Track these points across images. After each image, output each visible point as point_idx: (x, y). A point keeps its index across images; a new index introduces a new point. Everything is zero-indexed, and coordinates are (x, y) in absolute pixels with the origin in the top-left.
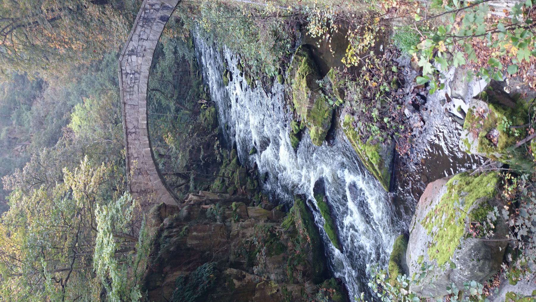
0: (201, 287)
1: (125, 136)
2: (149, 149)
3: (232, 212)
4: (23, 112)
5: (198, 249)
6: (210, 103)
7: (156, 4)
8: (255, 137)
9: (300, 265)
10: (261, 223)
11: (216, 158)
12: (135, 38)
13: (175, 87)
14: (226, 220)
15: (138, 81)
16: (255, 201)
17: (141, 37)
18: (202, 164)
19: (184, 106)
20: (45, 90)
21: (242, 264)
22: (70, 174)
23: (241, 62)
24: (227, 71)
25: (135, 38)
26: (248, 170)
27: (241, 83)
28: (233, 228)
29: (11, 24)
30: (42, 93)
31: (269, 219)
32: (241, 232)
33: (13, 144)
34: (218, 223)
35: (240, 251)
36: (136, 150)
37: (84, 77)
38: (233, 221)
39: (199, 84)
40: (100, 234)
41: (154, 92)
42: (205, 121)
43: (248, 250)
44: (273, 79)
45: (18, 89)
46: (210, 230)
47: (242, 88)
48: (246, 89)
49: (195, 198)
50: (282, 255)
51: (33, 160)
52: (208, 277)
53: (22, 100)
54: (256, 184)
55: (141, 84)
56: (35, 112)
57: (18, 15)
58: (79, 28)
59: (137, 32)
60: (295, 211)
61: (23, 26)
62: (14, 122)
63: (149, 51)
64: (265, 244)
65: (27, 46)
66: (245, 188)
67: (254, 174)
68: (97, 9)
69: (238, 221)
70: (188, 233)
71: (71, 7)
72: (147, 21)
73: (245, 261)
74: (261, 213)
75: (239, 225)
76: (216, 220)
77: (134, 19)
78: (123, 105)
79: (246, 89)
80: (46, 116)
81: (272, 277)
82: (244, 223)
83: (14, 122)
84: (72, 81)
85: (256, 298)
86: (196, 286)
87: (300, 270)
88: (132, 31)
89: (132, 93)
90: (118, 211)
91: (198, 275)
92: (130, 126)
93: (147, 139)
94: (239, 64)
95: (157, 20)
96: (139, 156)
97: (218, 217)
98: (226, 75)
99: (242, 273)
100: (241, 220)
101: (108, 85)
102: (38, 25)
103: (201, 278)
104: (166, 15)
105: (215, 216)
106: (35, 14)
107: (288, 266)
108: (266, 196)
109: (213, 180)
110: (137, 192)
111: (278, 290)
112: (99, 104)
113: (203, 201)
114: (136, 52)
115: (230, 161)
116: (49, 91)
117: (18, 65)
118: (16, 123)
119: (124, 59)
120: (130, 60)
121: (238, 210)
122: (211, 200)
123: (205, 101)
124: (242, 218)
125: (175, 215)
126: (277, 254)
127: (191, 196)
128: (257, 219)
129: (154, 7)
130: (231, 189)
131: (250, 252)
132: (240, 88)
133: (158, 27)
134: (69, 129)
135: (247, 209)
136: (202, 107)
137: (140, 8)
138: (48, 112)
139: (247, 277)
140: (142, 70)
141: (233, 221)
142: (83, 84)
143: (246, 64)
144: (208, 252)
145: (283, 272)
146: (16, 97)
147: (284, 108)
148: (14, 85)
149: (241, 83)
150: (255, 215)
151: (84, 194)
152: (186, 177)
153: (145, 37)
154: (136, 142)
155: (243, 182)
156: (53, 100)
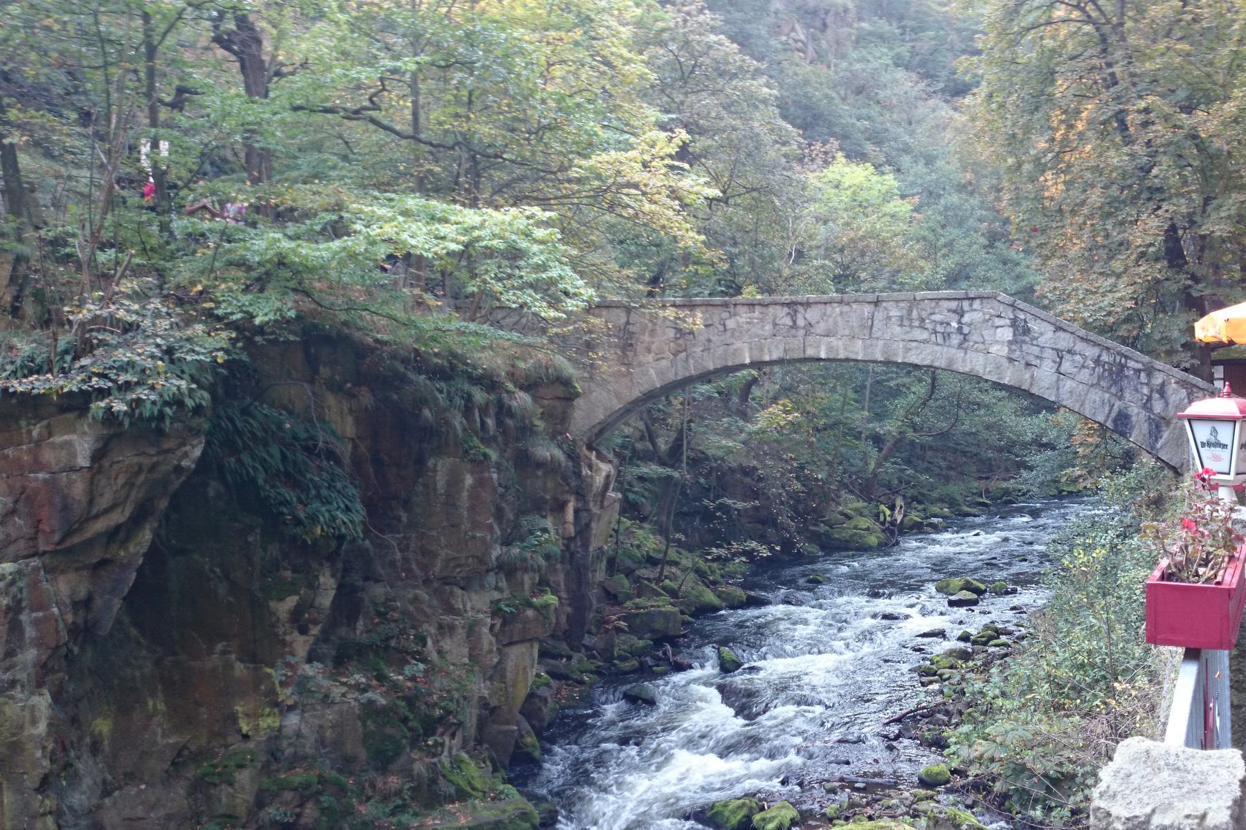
0: (290, 494)
1: (787, 298)
2: (747, 361)
3: (527, 593)
4: (891, 49)
5: (420, 488)
6: (892, 533)
7: (1167, 404)
8: (773, 668)
9: (317, 814)
10: (480, 688)
11: (718, 546)
12: (1064, 341)
13: (944, 435)
14: (502, 576)
15: (940, 340)
16: (574, 661)
17: (1067, 356)
18: (706, 502)
19: (886, 459)
20: (947, 101)
21: (351, 621)
22: (672, 149)
23: (1003, 639)
24: (979, 592)
25: (1064, 341)
26: (673, 641)
27: (941, 634)
28: (474, 597)
29: (1108, 22)
30: (940, 95)
31: (489, 712)
32: (459, 622)
33: (809, 21)
34: (496, 551)
35: (396, 615)
36: (745, 326)
37: (975, 201)
38: (496, 595)
39: (952, 503)
40: (470, 217)
41: (929, 381)
42: (842, 514)
43: (393, 643)
44: (939, 744)
45: (953, 37)
46: (476, 525)
47: (924, 635)
48: (920, 650)
49: (599, 480)
50: (363, 754)
51: (744, 61)
52: (313, 518)
53: (925, 46)
54: (626, 666)
55: (929, 348)
56: (889, 77)
57: (1132, 40)
58: (1098, 191)
59: (1080, 346)
60: (501, 805)
61: (1104, 51)
62: (865, 25)
63: (1027, 376)
64: (404, 698)
65: (1051, 58)
66: (619, 630)
67: (659, 659)
68: (1149, 240)
69: (496, 612)
70: (471, 461)
71: (1155, 171)
72: (1115, 375)
73: (360, 631)
74: (514, 686)
75: (481, 616)
76: (507, 542)
77: (1124, 341)
78: (870, 297)
79: (920, 650)
80: (878, 102)
81: (293, 720)
82: (485, 630)
83: (865, 25)
84: (965, 169)
85: (229, 666)
86: (292, 478)
87: (299, 816)
88: (1083, 333)
89: (906, 323)
90: (543, 267)
91: (329, 488)
92: (813, 314)
93: (775, 357)
94: (999, 633)
95: (1118, 404)
96: (729, 334)
97: (515, 551)
98: (968, 587)
99: (315, 622)
100: (498, 622)
101: (950, 263)
102: (1108, 87)
103: (318, 496)
104: (1132, 428)
105: (522, 541)
106: (1136, 79)
107: (320, 776)
108: (582, 699)
109: (661, 530)
110: (628, 323)
111: (246, 737)
112: (896, 235)
113: (586, 502)
114: (1024, 342)
115: (714, 583)
116: (945, 112)
117: (999, 34)
118: (862, 29)
119: (1002, 307)
120: (998, 322)
121: (530, 613)
122: (588, 525)
123: (899, 518)
124: (503, 625)
125: (540, 424)
126: (367, 736)
127: (605, 468)
128: (496, 673)
129: (1156, 396)
130: (623, 584)
131: (387, 648)
132: (926, 630)
133: (1098, 405)
134: (834, 158)
135: (531, 640)
136: (883, 507)
137: (1158, 357)
138: (890, 108)
139: (301, 639)
140: (970, 353)
141: (496, 595)
142: (955, 199)
143: (994, 655)
144: (404, 517)
145: (305, 758)
146: (931, 33)
147: (842, 779)
148: (965, 30)
149: (941, 634)
150: (510, 665)
151: (611, 181)
152: (674, 456)
153: (1066, 366)
154: (768, 327)
155: (636, 624)
156: (919, 122)
